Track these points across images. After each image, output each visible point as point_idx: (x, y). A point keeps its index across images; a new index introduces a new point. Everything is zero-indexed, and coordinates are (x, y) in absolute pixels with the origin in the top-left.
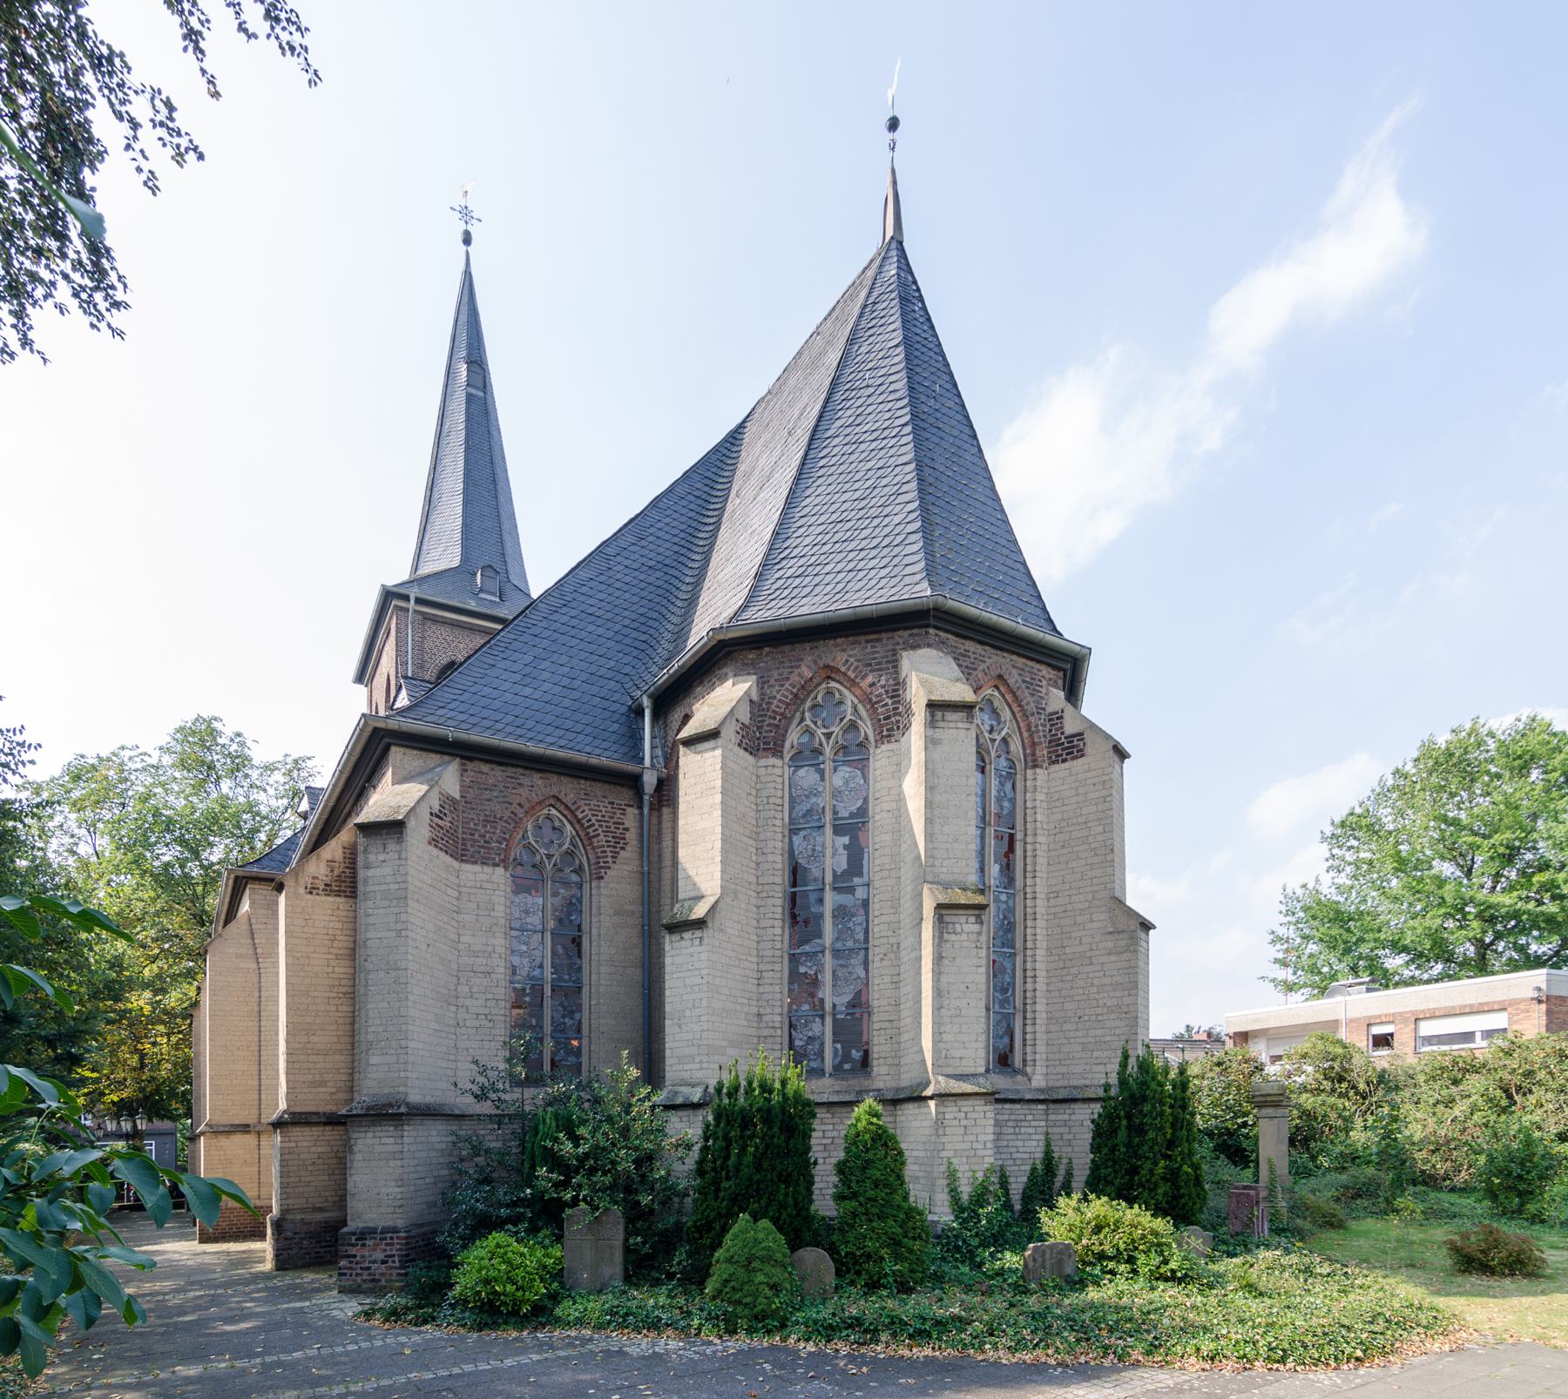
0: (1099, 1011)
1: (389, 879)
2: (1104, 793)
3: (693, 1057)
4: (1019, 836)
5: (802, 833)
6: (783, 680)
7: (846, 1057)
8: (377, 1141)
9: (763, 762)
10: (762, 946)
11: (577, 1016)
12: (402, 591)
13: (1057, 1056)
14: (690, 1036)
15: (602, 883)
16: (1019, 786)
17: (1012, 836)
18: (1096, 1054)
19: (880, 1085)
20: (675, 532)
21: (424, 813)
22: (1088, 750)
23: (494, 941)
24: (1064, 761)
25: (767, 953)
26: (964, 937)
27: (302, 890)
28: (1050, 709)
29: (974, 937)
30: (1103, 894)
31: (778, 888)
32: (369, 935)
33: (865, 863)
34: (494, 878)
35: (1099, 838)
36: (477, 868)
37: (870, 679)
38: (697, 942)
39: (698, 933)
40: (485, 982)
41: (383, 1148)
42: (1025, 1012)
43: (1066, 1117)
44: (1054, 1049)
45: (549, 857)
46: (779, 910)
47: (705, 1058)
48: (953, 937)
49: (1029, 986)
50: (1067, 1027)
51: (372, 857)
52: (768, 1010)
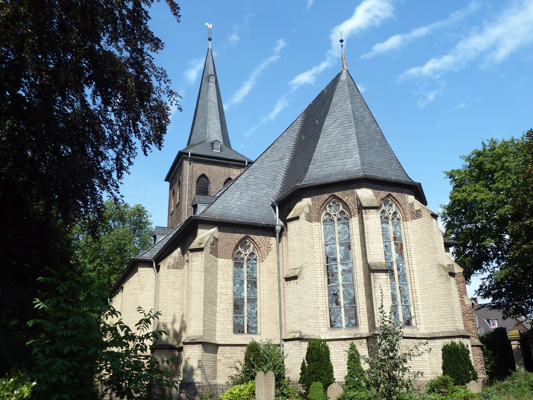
0: (440, 304)
1: (199, 265)
2: (430, 229)
3: (296, 322)
4: (404, 244)
5: (329, 246)
6: (318, 200)
7: (349, 323)
8: (193, 351)
9: (314, 224)
10: (317, 284)
11: (256, 309)
12: (184, 151)
13: (428, 321)
14: (295, 315)
15: (263, 263)
16: (402, 227)
17: (401, 244)
18: (441, 320)
19: (362, 332)
20: (284, 148)
21: (209, 244)
22: (423, 215)
23: (228, 284)
24: (416, 219)
25: (319, 286)
26: (382, 280)
27: (166, 268)
28: (409, 202)
29: (385, 280)
30: (435, 263)
31: (322, 264)
32: (192, 283)
33: (350, 255)
34: (229, 263)
35: (431, 244)
36: (223, 260)
37: (346, 198)
38: (295, 283)
39: (296, 281)
40: (226, 297)
41: (194, 354)
42: (414, 305)
43: (434, 344)
44: (427, 318)
45: (246, 255)
46: (323, 271)
47: (300, 322)
48: (378, 280)
49: (414, 296)
50: (430, 310)
51: (193, 259)
52: (321, 306)
